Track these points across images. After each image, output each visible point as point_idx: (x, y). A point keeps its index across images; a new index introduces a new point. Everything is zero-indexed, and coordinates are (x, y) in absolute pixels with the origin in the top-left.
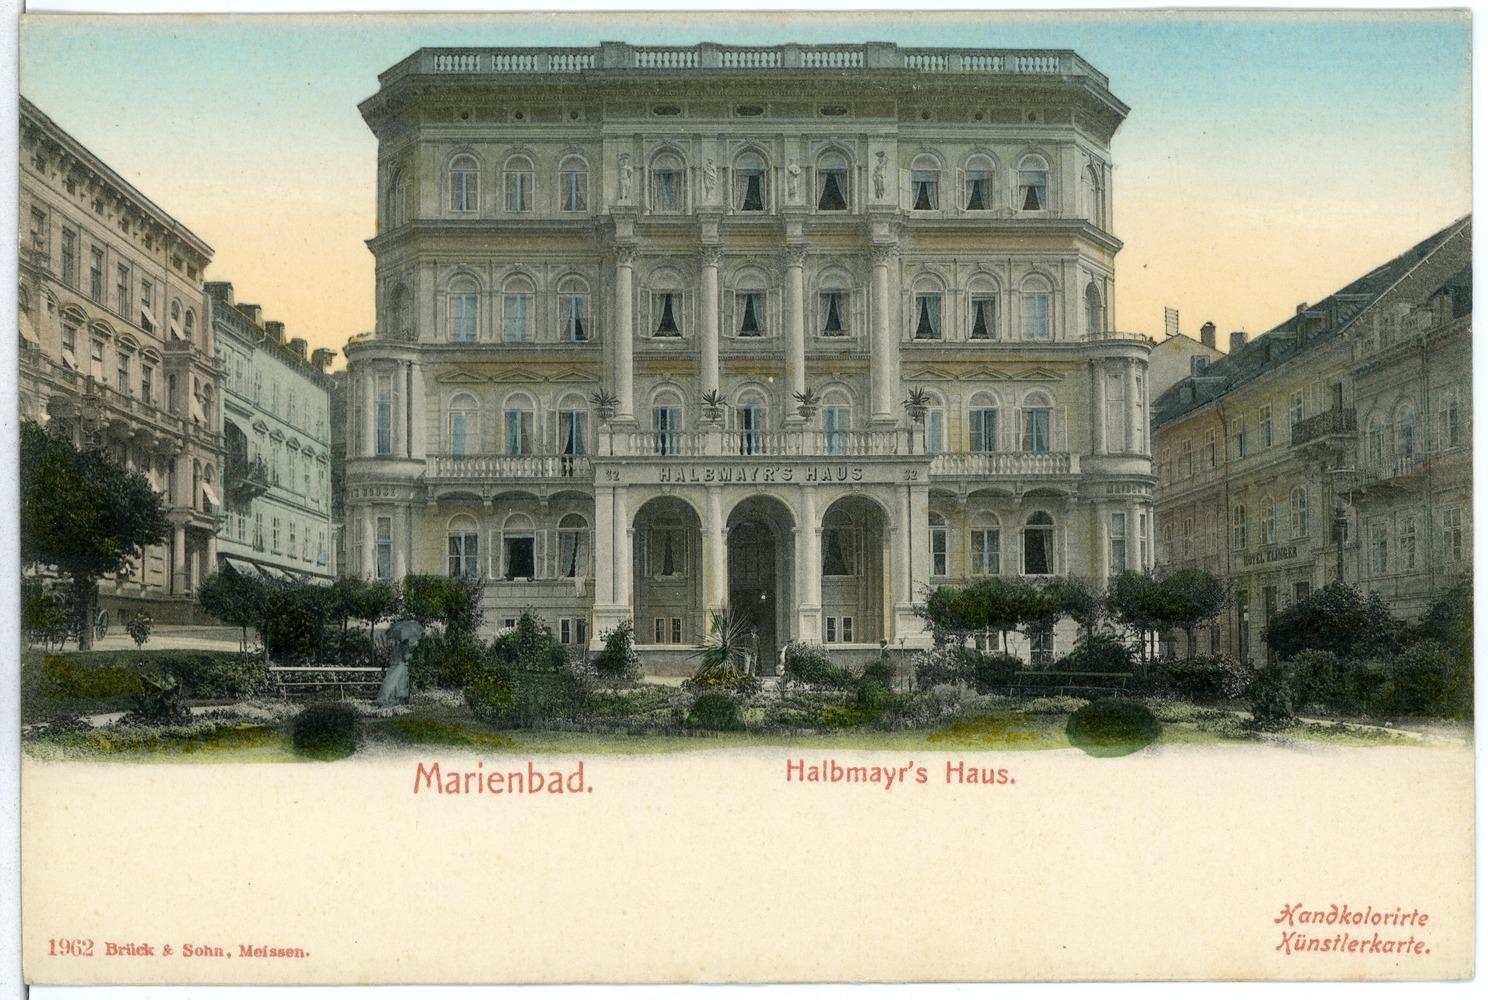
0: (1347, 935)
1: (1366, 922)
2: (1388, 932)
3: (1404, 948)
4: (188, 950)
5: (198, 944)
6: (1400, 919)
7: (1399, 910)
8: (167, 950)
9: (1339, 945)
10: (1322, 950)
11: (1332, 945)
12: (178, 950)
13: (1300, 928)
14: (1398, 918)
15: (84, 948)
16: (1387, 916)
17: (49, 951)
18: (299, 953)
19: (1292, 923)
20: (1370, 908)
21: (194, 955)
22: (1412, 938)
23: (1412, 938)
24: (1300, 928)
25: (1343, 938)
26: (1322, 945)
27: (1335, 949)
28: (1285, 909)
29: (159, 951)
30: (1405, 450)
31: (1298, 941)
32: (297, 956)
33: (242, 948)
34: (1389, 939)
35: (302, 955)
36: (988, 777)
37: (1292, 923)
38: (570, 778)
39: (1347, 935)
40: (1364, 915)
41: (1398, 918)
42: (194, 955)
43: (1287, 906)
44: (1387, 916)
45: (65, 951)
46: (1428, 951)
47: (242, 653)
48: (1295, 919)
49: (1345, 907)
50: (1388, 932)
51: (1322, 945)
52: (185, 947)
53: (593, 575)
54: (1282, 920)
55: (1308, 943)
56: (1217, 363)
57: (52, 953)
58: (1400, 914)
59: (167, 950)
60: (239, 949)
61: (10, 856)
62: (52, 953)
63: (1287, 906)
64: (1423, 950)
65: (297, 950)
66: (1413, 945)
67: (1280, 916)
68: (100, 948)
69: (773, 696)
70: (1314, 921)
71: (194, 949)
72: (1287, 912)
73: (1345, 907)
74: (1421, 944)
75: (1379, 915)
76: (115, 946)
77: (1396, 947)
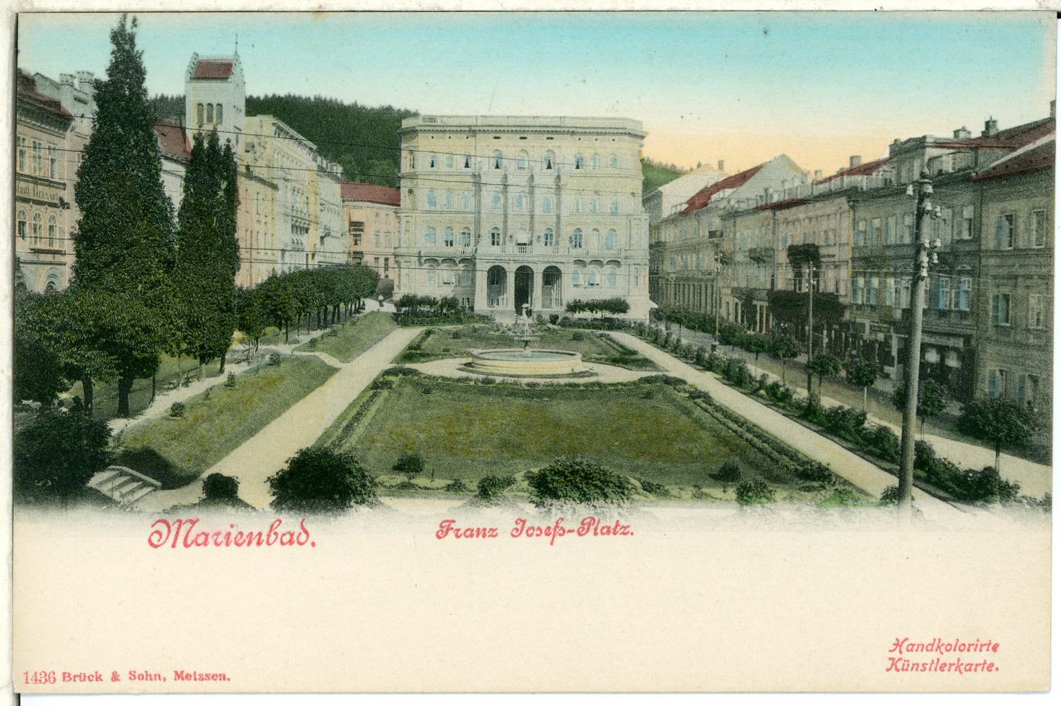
0: (938, 660)
1: (955, 650)
2: (967, 658)
3: (979, 668)
4: (132, 675)
5: (140, 671)
6: (979, 647)
7: (978, 641)
8: (115, 677)
9: (934, 666)
10: (922, 670)
11: (928, 667)
12: (124, 676)
13: (906, 655)
14: (978, 646)
15: (49, 678)
16: (970, 645)
17: (25, 681)
18: (223, 677)
19: (901, 652)
20: (958, 640)
21: (137, 680)
22: (985, 661)
23: (985, 661)
24: (906, 655)
25: (935, 662)
26: (921, 667)
27: (930, 670)
28: (896, 642)
29: (107, 677)
30: (250, 360)
31: (904, 665)
32: (220, 679)
33: (176, 673)
34: (968, 662)
35: (224, 678)
36: (157, 677)
37: (901, 652)
38: (275, 541)
39: (938, 660)
40: (953, 645)
41: (978, 646)
42: (137, 680)
43: (897, 639)
44: (970, 645)
45: (52, 675)
46: (997, 669)
47: (331, 162)
48: (904, 650)
49: (940, 640)
50: (967, 658)
51: (921, 667)
52: (130, 673)
53: (472, 117)
54: (895, 650)
55: (911, 666)
56: (93, 141)
57: (27, 682)
58: (979, 644)
59: (115, 677)
60: (174, 674)
61: (7, 550)
62: (27, 682)
63: (897, 639)
64: (993, 669)
65: (220, 675)
66: (986, 666)
67: (893, 647)
68: (59, 677)
69: (983, 255)
70: (917, 650)
71: (137, 675)
72: (898, 644)
73: (940, 640)
74: (992, 665)
75: (964, 645)
76: (69, 674)
77: (973, 667)
